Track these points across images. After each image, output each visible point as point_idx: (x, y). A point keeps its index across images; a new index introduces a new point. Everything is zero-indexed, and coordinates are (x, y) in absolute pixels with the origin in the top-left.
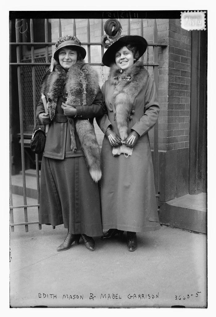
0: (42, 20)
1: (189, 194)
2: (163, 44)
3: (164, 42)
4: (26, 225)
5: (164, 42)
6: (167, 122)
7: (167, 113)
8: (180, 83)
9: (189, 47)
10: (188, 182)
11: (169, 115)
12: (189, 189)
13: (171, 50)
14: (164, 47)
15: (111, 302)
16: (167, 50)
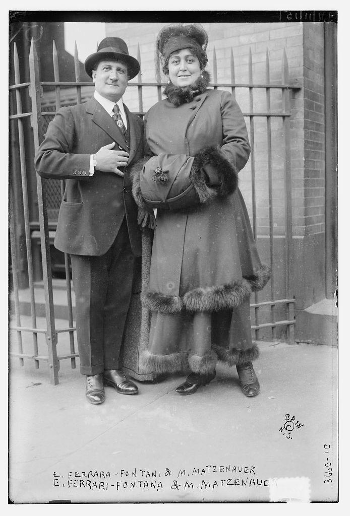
0: (58, 24)
1: (327, 298)
2: (296, 86)
3: (296, 83)
4: (72, 359)
5: (296, 83)
6: (303, 195)
7: (303, 183)
8: (315, 140)
9: (323, 90)
10: (324, 279)
11: (305, 186)
12: (326, 293)
13: (307, 94)
14: (296, 90)
15: (139, 493)
16: (302, 93)
